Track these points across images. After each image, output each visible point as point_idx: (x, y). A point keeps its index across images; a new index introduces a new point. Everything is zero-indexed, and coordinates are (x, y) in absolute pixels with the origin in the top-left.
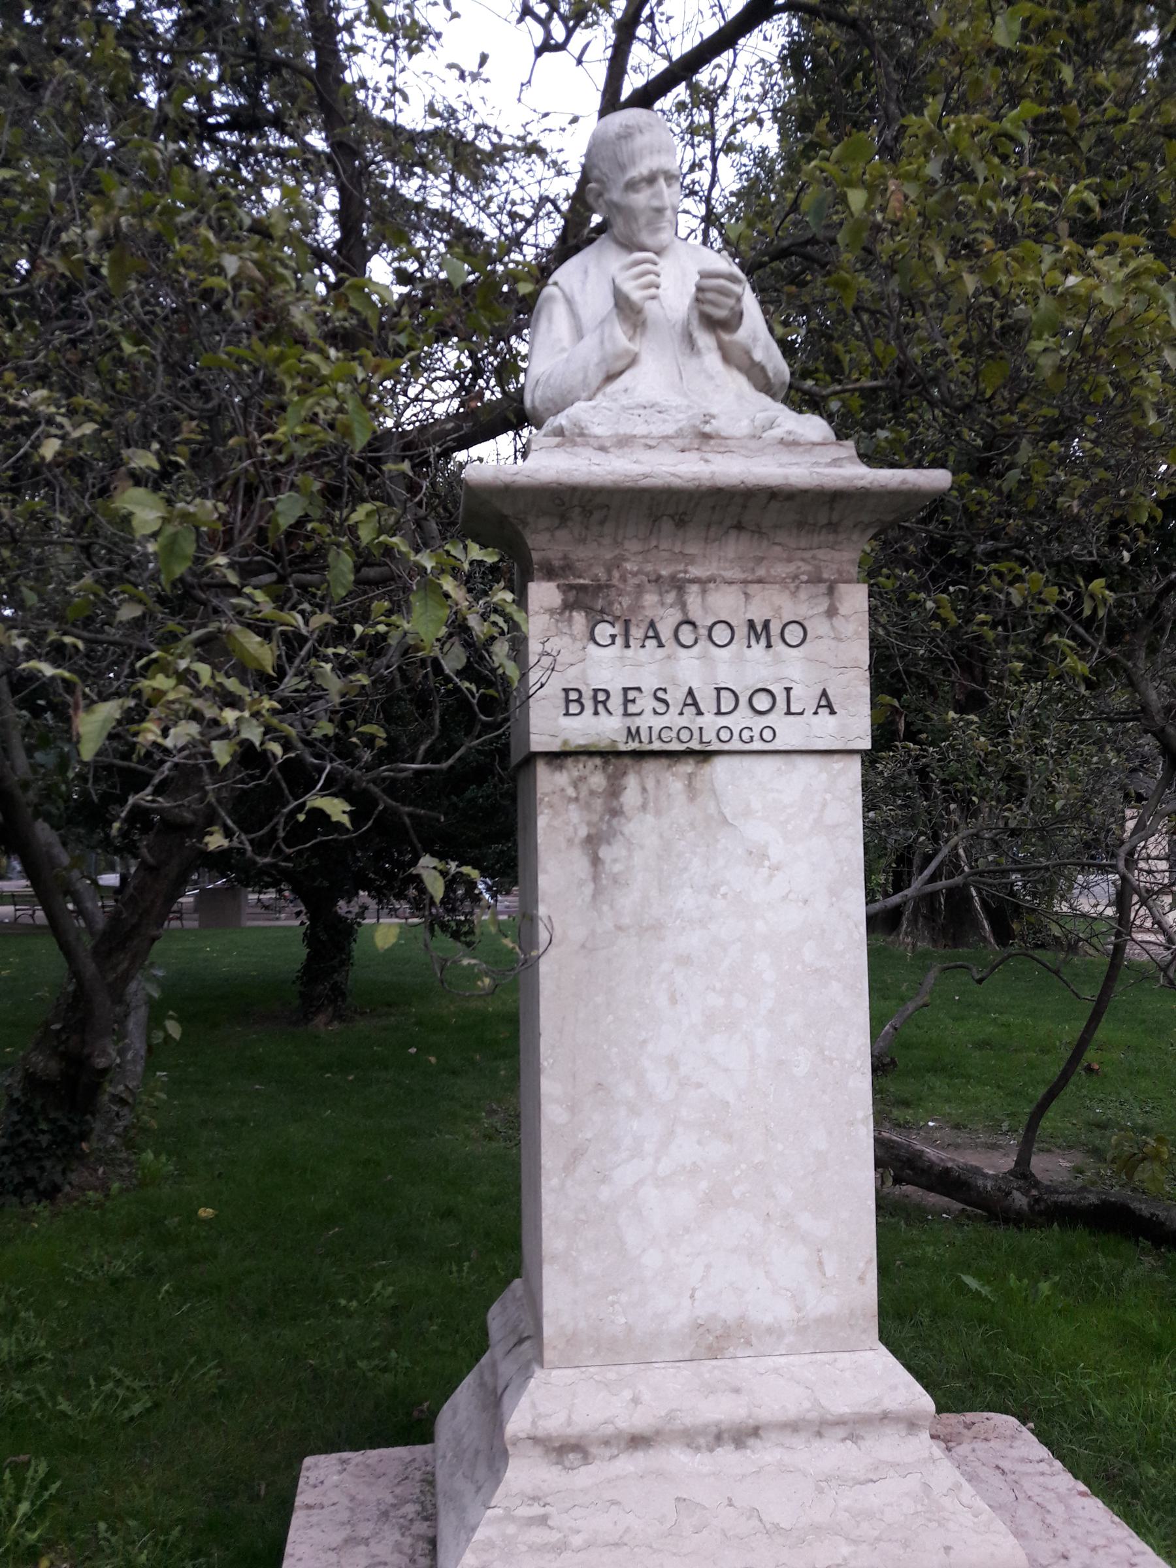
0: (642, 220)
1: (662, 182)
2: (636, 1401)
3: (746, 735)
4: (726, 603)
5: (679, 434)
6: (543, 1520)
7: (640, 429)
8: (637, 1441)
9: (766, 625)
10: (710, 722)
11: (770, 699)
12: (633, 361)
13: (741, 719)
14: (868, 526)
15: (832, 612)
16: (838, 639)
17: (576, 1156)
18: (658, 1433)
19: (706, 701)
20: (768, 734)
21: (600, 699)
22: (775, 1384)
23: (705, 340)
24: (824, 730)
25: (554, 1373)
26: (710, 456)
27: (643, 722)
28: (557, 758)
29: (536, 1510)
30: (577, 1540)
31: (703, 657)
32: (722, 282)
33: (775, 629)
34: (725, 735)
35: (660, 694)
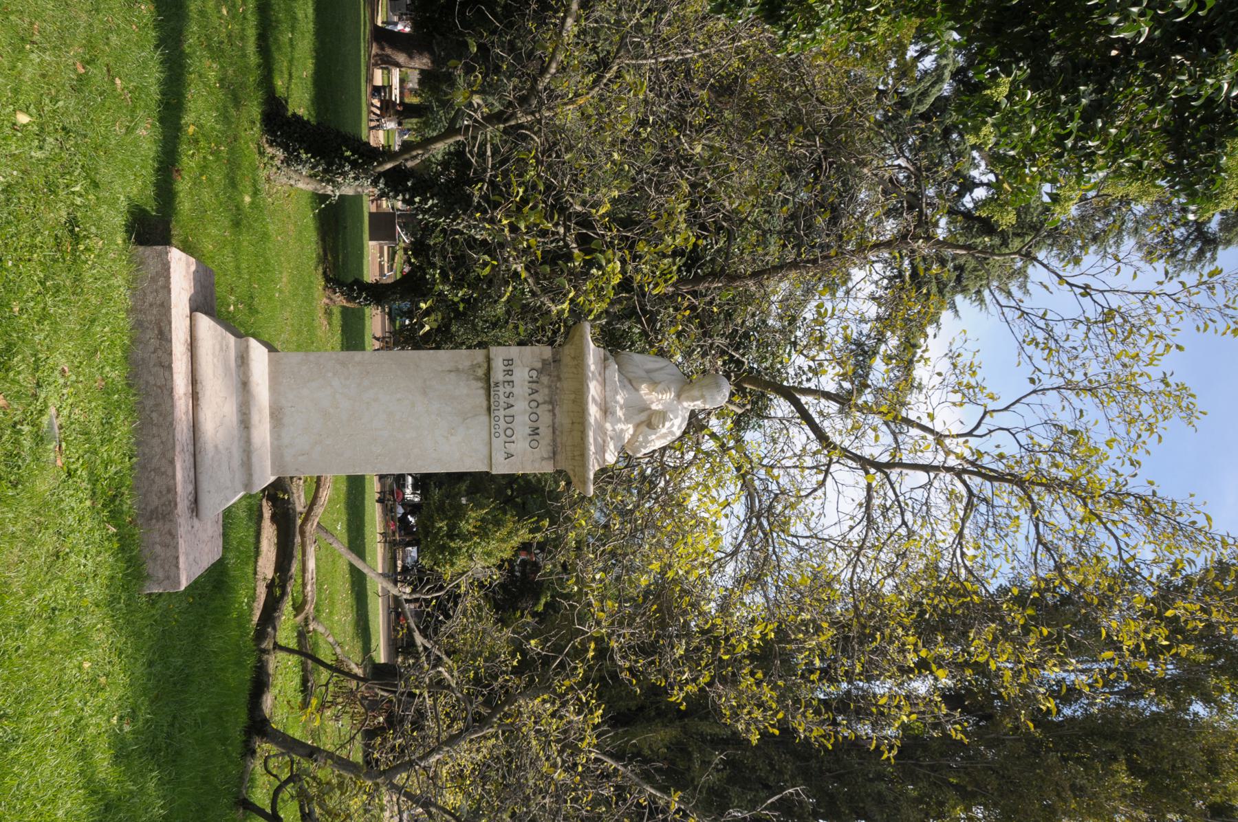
10: (502, 413)
13: (502, 423)
15: (543, 459)
17: (343, 364)
19: (509, 412)
21: (509, 372)
24: (499, 457)
27: (501, 389)
28: (489, 360)
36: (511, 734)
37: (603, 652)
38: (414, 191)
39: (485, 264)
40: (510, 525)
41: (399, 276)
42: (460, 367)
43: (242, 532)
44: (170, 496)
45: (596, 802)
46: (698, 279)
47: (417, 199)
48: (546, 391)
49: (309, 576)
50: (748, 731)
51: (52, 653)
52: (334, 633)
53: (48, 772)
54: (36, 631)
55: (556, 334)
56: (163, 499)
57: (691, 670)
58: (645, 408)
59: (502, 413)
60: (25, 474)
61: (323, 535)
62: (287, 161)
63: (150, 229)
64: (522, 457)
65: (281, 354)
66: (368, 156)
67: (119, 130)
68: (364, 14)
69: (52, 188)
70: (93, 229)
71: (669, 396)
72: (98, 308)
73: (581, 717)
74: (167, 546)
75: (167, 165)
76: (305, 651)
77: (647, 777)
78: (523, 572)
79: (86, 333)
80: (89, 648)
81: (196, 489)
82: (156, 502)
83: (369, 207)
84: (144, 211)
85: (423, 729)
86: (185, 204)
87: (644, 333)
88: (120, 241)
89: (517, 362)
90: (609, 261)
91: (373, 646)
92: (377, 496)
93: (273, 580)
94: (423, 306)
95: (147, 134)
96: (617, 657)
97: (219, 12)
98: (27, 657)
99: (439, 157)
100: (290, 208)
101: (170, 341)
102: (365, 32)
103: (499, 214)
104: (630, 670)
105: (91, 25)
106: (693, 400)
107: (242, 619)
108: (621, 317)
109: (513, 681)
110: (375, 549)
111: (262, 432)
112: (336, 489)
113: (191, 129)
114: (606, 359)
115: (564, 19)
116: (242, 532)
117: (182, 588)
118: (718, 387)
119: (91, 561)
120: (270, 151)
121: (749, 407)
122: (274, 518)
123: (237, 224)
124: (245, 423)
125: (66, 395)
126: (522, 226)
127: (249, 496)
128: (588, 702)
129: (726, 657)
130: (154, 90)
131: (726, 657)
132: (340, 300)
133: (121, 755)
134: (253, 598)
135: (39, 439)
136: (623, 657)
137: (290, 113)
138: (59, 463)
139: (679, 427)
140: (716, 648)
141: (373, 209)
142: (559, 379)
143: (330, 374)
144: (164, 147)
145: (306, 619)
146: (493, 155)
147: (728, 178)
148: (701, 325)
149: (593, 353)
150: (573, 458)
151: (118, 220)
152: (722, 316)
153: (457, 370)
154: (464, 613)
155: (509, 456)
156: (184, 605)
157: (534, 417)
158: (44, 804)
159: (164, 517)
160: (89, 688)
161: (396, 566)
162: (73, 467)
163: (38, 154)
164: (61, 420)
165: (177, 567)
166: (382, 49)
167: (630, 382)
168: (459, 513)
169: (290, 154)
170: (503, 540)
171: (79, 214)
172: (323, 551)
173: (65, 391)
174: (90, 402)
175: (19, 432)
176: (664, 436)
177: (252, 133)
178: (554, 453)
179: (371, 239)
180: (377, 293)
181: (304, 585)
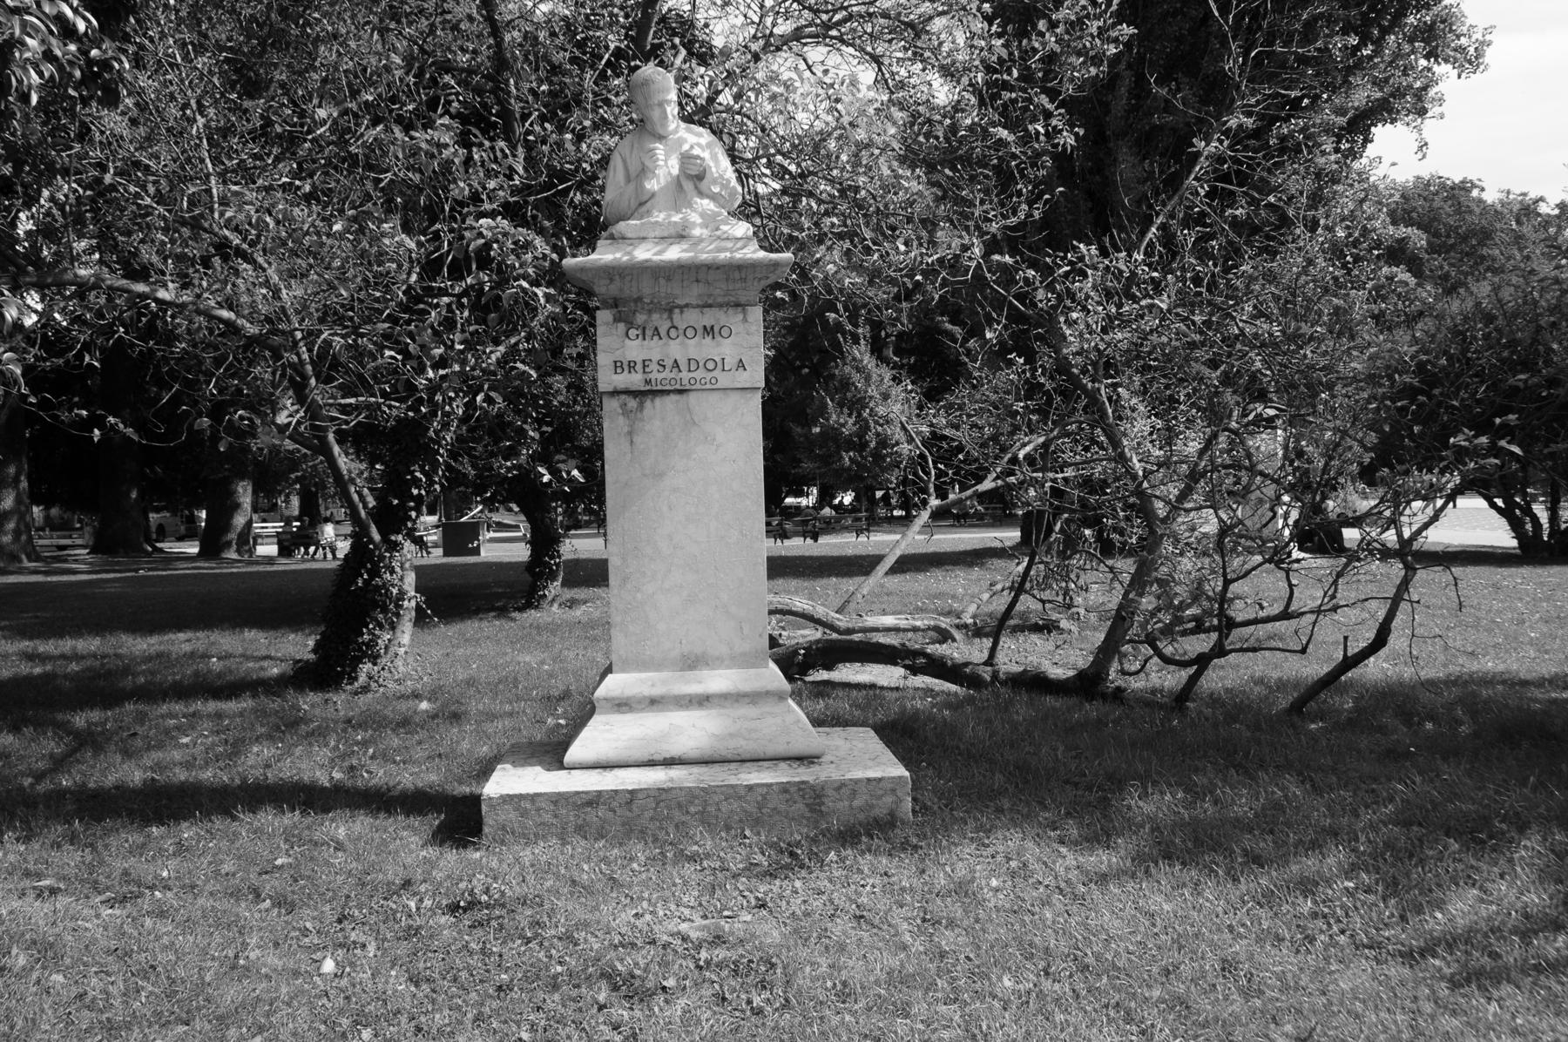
10: (685, 375)
13: (699, 374)
15: (745, 320)
17: (625, 580)
18: (663, 697)
19: (683, 367)
21: (632, 366)
24: (743, 379)
27: (653, 376)
28: (615, 393)
31: (682, 344)
33: (716, 329)
36: (1107, 366)
37: (1010, 241)
38: (405, 496)
39: (489, 400)
40: (847, 369)
41: (523, 518)
42: (626, 429)
43: (841, 704)
44: (793, 789)
45: (1202, 254)
46: (506, 114)
47: (415, 492)
48: (655, 316)
49: (903, 624)
50: (1116, 41)
51: (977, 921)
52: (976, 594)
53: (1117, 923)
54: (947, 939)
55: (582, 301)
56: (796, 797)
57: (1034, 120)
58: (678, 184)
59: (685, 375)
60: (758, 954)
61: (852, 606)
62: (374, 659)
63: (460, 820)
64: (744, 348)
65: (614, 658)
66: (361, 554)
67: (339, 859)
68: (183, 569)
69: (412, 932)
70: (462, 885)
71: (660, 149)
72: (557, 876)
73: (1090, 272)
74: (854, 792)
75: (380, 801)
76: (995, 628)
77: (1173, 183)
78: (910, 353)
79: (589, 890)
80: (973, 880)
81: (784, 759)
82: (801, 806)
83: (437, 556)
84: (439, 827)
85: (1105, 481)
86: (428, 777)
87: (580, 186)
88: (477, 855)
89: (618, 356)
90: (480, 235)
91: (998, 544)
92: (809, 541)
93: (906, 667)
94: (546, 479)
95: (341, 827)
96: (1013, 221)
97: (187, 745)
98: (979, 948)
99: (363, 466)
100: (436, 653)
101: (600, 792)
102: (207, 568)
103: (421, 382)
104: (1030, 204)
105: (211, 894)
106: (666, 117)
107: (954, 704)
108: (559, 219)
109: (1046, 360)
110: (876, 542)
111: (718, 681)
112: (796, 592)
113: (337, 775)
114: (612, 237)
115: (157, 300)
116: (841, 704)
117: (907, 774)
118: (646, 83)
119: (870, 877)
120: (363, 678)
121: (677, 41)
122: (829, 668)
123: (456, 717)
124: (703, 701)
125: (668, 910)
126: (438, 351)
127: (797, 695)
128: (1071, 263)
129: (1015, 73)
130: (291, 818)
131: (1015, 73)
132: (554, 588)
133: (1098, 838)
134: (929, 691)
135: (718, 940)
136: (1015, 213)
137: (312, 656)
138: (749, 918)
139: (700, 135)
140: (1006, 86)
141: (440, 551)
142: (639, 299)
143: (639, 596)
144: (359, 807)
145: (958, 627)
146: (356, 396)
147: (365, 70)
148: (567, 109)
149: (605, 254)
150: (744, 280)
151: (450, 858)
152: (555, 79)
153: (630, 433)
154: (957, 427)
155: (741, 365)
156: (930, 772)
157: (690, 333)
158: (1154, 925)
159: (819, 797)
160: (1014, 876)
161: (900, 517)
162: (753, 902)
163: (371, 950)
164: (696, 917)
165: (880, 780)
166: (229, 544)
167: (641, 204)
168: (832, 436)
169: (365, 655)
170: (868, 379)
171: (444, 902)
172: (874, 607)
173: (661, 913)
174: (675, 885)
175: (708, 962)
176: (714, 157)
177: (340, 701)
178: (737, 305)
179: (476, 551)
180: (544, 541)
181: (915, 629)
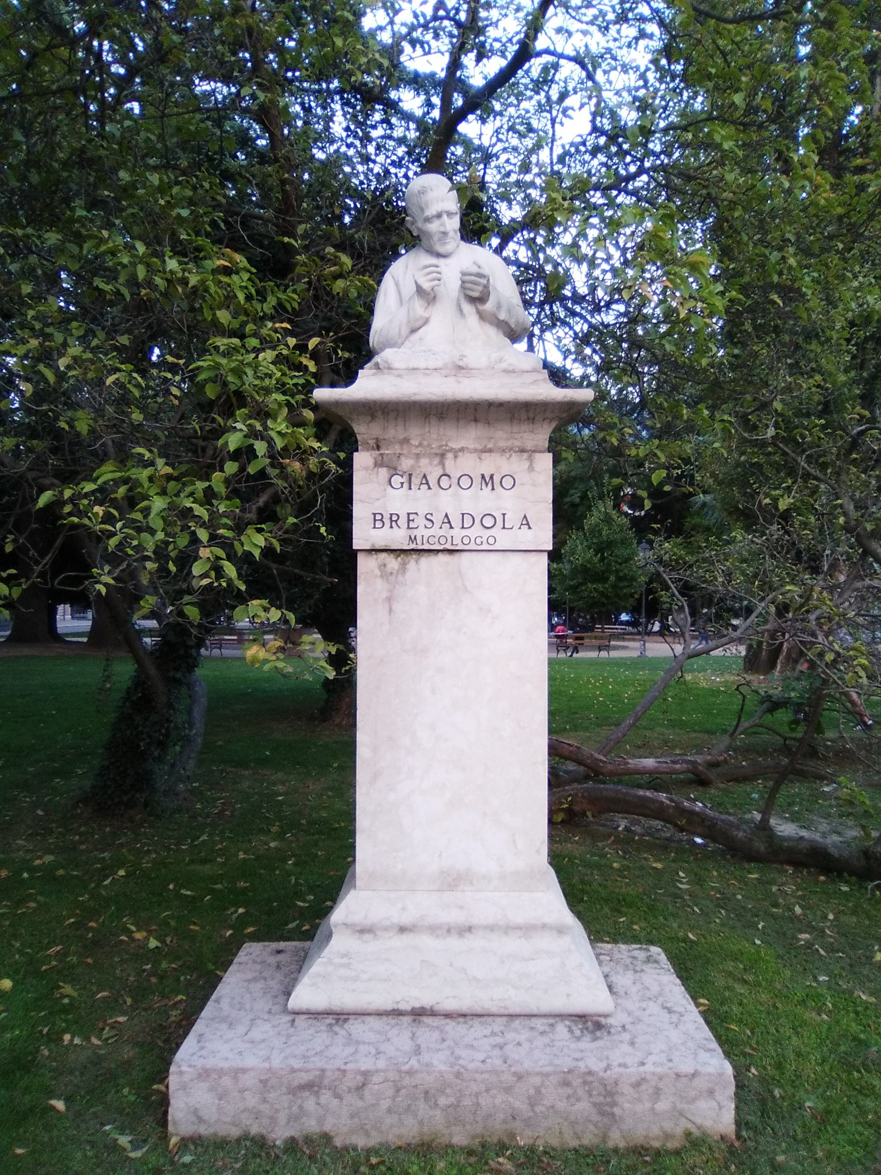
0: (436, 238)
1: (445, 216)
2: (404, 909)
3: (478, 541)
4: (468, 464)
5: (444, 367)
6: (347, 966)
7: (422, 365)
8: (403, 930)
9: (492, 477)
10: (457, 533)
11: (493, 520)
12: (426, 321)
13: (476, 531)
14: (551, 420)
15: (531, 469)
16: (534, 485)
17: (376, 776)
18: (414, 926)
19: (456, 521)
20: (491, 541)
21: (394, 520)
22: (483, 906)
23: (468, 308)
25: (362, 893)
26: (461, 379)
27: (418, 533)
29: (345, 960)
30: (364, 976)
32: (473, 278)
33: (497, 479)
34: (466, 541)
35: (429, 517)
42: (385, 595)
44: (577, 1082)
48: (424, 461)
56: (580, 1092)
74: (657, 1092)
89: (377, 508)
153: (389, 600)
157: (465, 482)
159: (610, 1094)
178: (523, 451)
